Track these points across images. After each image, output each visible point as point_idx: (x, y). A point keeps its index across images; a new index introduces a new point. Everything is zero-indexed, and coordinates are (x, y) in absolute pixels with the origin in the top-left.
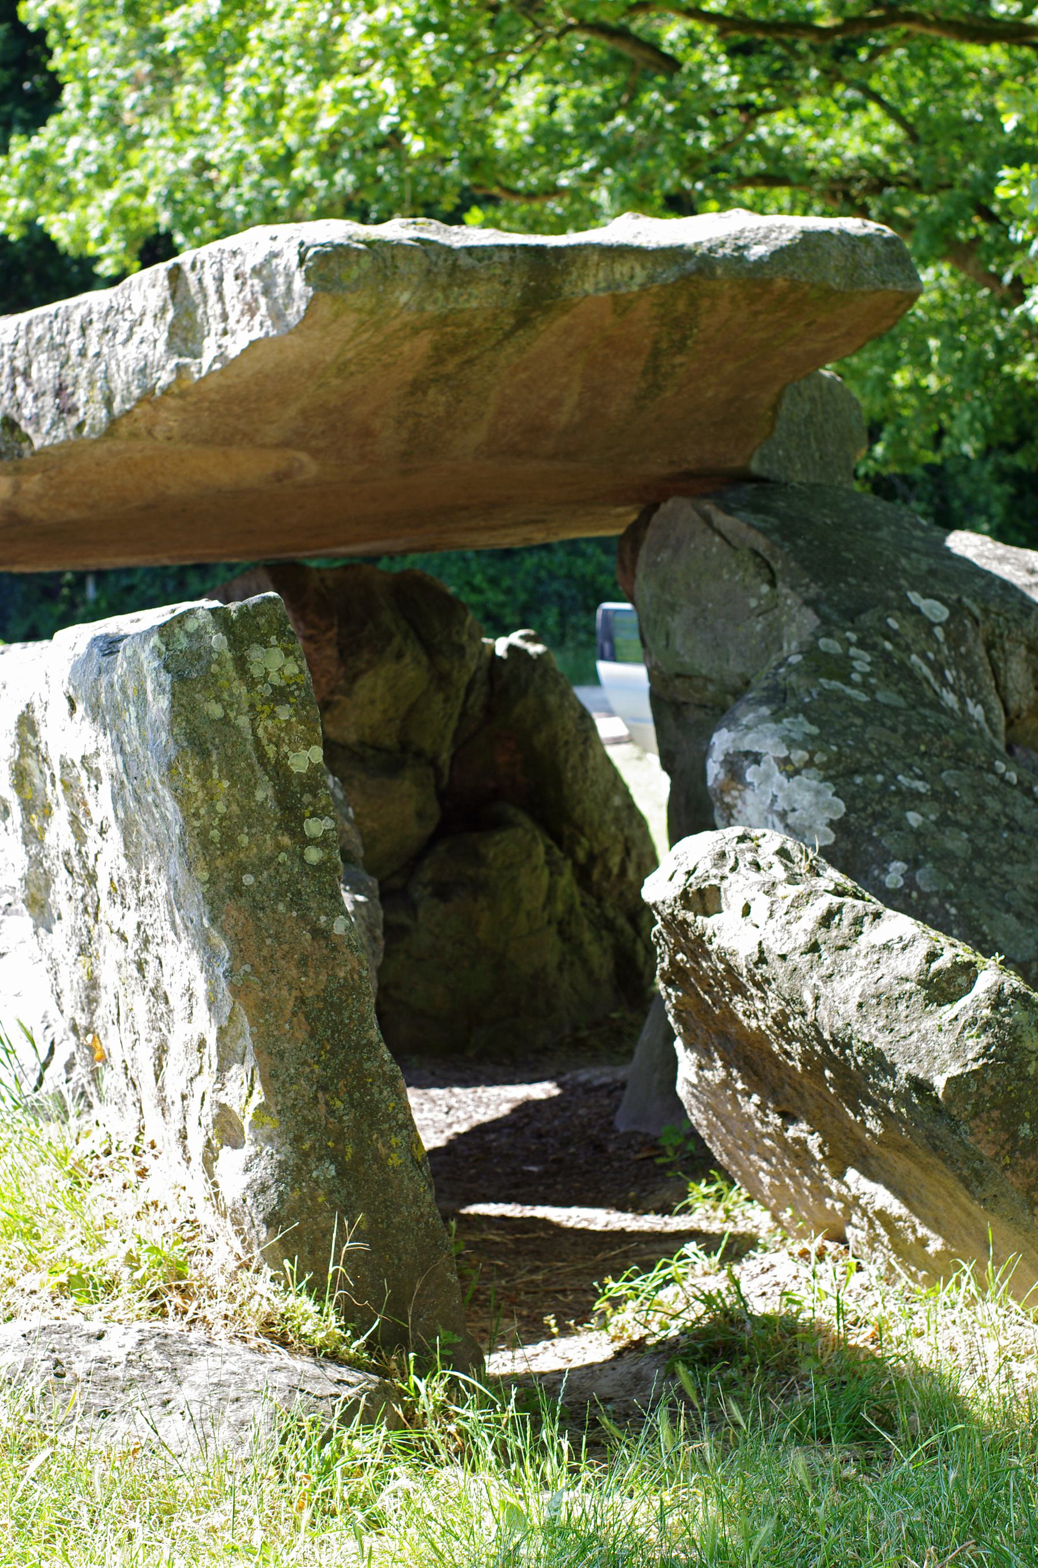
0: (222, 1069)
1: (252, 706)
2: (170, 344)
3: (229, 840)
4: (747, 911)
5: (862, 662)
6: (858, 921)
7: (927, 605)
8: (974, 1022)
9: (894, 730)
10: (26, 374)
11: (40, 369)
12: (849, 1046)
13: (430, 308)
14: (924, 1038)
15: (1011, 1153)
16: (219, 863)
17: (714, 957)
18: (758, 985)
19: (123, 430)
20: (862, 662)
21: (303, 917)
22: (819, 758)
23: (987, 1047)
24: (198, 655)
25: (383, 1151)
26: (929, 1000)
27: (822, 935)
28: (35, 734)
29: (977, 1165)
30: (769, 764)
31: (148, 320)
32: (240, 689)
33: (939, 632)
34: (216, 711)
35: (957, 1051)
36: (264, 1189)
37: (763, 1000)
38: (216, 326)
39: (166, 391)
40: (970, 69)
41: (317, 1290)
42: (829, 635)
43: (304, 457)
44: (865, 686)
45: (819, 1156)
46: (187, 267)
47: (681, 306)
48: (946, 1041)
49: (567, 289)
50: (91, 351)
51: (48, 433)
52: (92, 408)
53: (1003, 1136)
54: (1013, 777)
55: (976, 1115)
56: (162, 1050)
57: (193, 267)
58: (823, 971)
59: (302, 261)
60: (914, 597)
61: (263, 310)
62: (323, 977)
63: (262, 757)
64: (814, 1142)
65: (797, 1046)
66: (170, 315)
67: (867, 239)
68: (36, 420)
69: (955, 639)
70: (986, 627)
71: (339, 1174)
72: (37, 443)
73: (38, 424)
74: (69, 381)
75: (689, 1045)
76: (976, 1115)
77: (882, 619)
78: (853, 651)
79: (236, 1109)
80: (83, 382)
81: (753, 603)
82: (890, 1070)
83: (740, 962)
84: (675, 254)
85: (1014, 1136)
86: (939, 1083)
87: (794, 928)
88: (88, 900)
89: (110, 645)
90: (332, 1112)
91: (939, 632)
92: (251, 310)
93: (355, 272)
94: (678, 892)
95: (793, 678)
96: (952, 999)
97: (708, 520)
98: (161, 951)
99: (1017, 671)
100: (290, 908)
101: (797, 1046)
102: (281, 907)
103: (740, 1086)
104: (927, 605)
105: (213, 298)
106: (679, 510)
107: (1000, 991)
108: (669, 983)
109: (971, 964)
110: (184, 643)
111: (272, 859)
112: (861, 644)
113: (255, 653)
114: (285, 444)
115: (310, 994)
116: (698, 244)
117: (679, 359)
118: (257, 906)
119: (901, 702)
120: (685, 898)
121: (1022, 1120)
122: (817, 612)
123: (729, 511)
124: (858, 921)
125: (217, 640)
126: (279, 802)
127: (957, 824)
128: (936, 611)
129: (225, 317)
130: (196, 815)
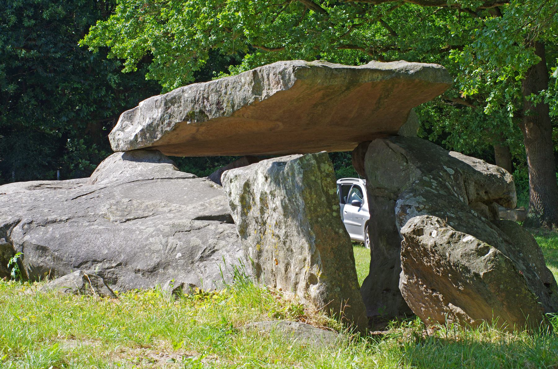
0: (312, 265)
1: (321, 178)
2: (253, 92)
3: (315, 210)
4: (431, 234)
5: (435, 183)
6: (459, 236)
7: (448, 169)
8: (489, 260)
9: (445, 201)
10: (207, 99)
11: (212, 97)
12: (458, 266)
13: (325, 84)
14: (477, 264)
15: (498, 292)
16: (313, 215)
17: (421, 247)
18: (433, 253)
19: (236, 115)
20: (435, 183)
21: (332, 229)
22: (427, 207)
23: (493, 266)
24: (310, 165)
25: (351, 286)
26: (478, 255)
27: (451, 240)
28: (249, 187)
29: (490, 295)
30: (413, 208)
31: (246, 86)
32: (319, 174)
33: (452, 177)
34: (313, 178)
35: (486, 267)
36: (323, 293)
37: (434, 257)
38: (266, 87)
39: (251, 104)
40: (411, 11)
41: (337, 317)
42: (425, 176)
43: (280, 124)
44: (436, 189)
45: (442, 300)
46: (258, 71)
47: (390, 85)
48: (483, 265)
49: (360, 80)
50: (228, 93)
51: (214, 115)
52: (228, 108)
53: (497, 288)
54: (476, 214)
55: (490, 282)
56: (287, 265)
57: (260, 71)
58: (451, 248)
59: (294, 71)
60: (445, 167)
61: (281, 83)
62: (337, 243)
63: (323, 190)
64: (440, 296)
65: (442, 269)
66: (253, 84)
67: (439, 69)
68: (210, 111)
69: (456, 179)
70: (464, 176)
71: (341, 290)
72: (210, 117)
73: (211, 112)
74: (221, 101)
75: (406, 273)
76: (490, 282)
77: (438, 173)
78: (432, 180)
79: (316, 274)
80: (225, 101)
81: (401, 168)
82: (469, 271)
83: (429, 247)
84: (390, 72)
85: (499, 288)
86: (482, 274)
87: (444, 238)
88: (262, 229)
89: (281, 165)
90: (339, 275)
91: (452, 177)
92: (278, 83)
93: (307, 74)
94: (412, 230)
95: (417, 187)
96: (484, 255)
97: (388, 145)
98: (292, 238)
99: (472, 189)
100: (329, 226)
101: (442, 269)
102: (327, 226)
103: (420, 283)
104: (448, 169)
105: (266, 80)
106: (378, 143)
107: (496, 253)
108: (404, 256)
109: (488, 247)
110: (305, 162)
111: (325, 215)
112: (433, 179)
113: (322, 165)
114: (277, 120)
115: (334, 247)
116: (396, 69)
117: (386, 100)
118: (322, 226)
119: (445, 194)
120: (414, 232)
121: (501, 284)
122: (421, 170)
123: (394, 143)
124: (459, 236)
125: (313, 161)
126: (327, 201)
127: (463, 226)
128: (452, 172)
129: (269, 85)
130: (308, 203)
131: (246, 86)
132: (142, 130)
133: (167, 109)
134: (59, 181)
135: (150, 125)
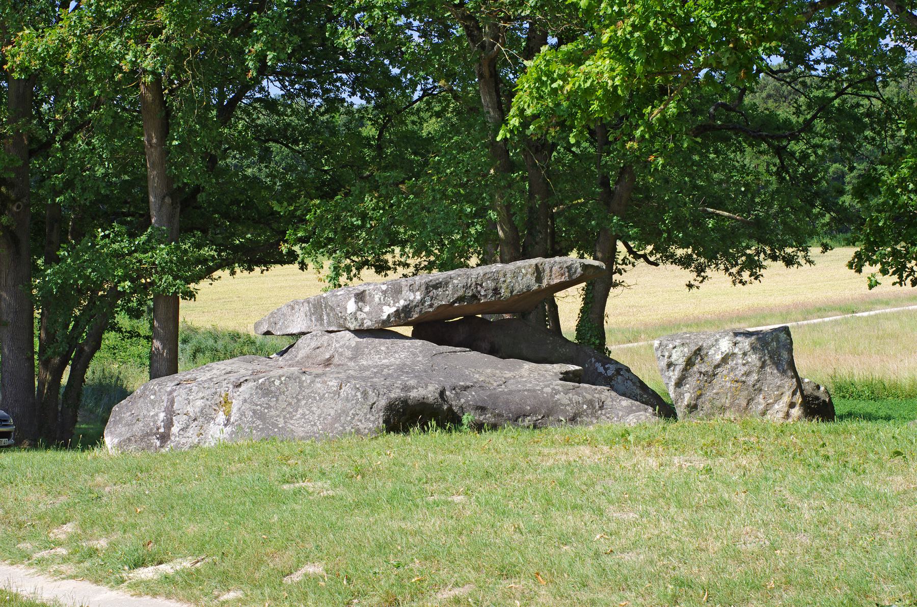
10: (481, 285)
31: (529, 276)
131: (529, 276)
132: (397, 311)
133: (428, 293)
134: (577, 384)
135: (405, 307)
